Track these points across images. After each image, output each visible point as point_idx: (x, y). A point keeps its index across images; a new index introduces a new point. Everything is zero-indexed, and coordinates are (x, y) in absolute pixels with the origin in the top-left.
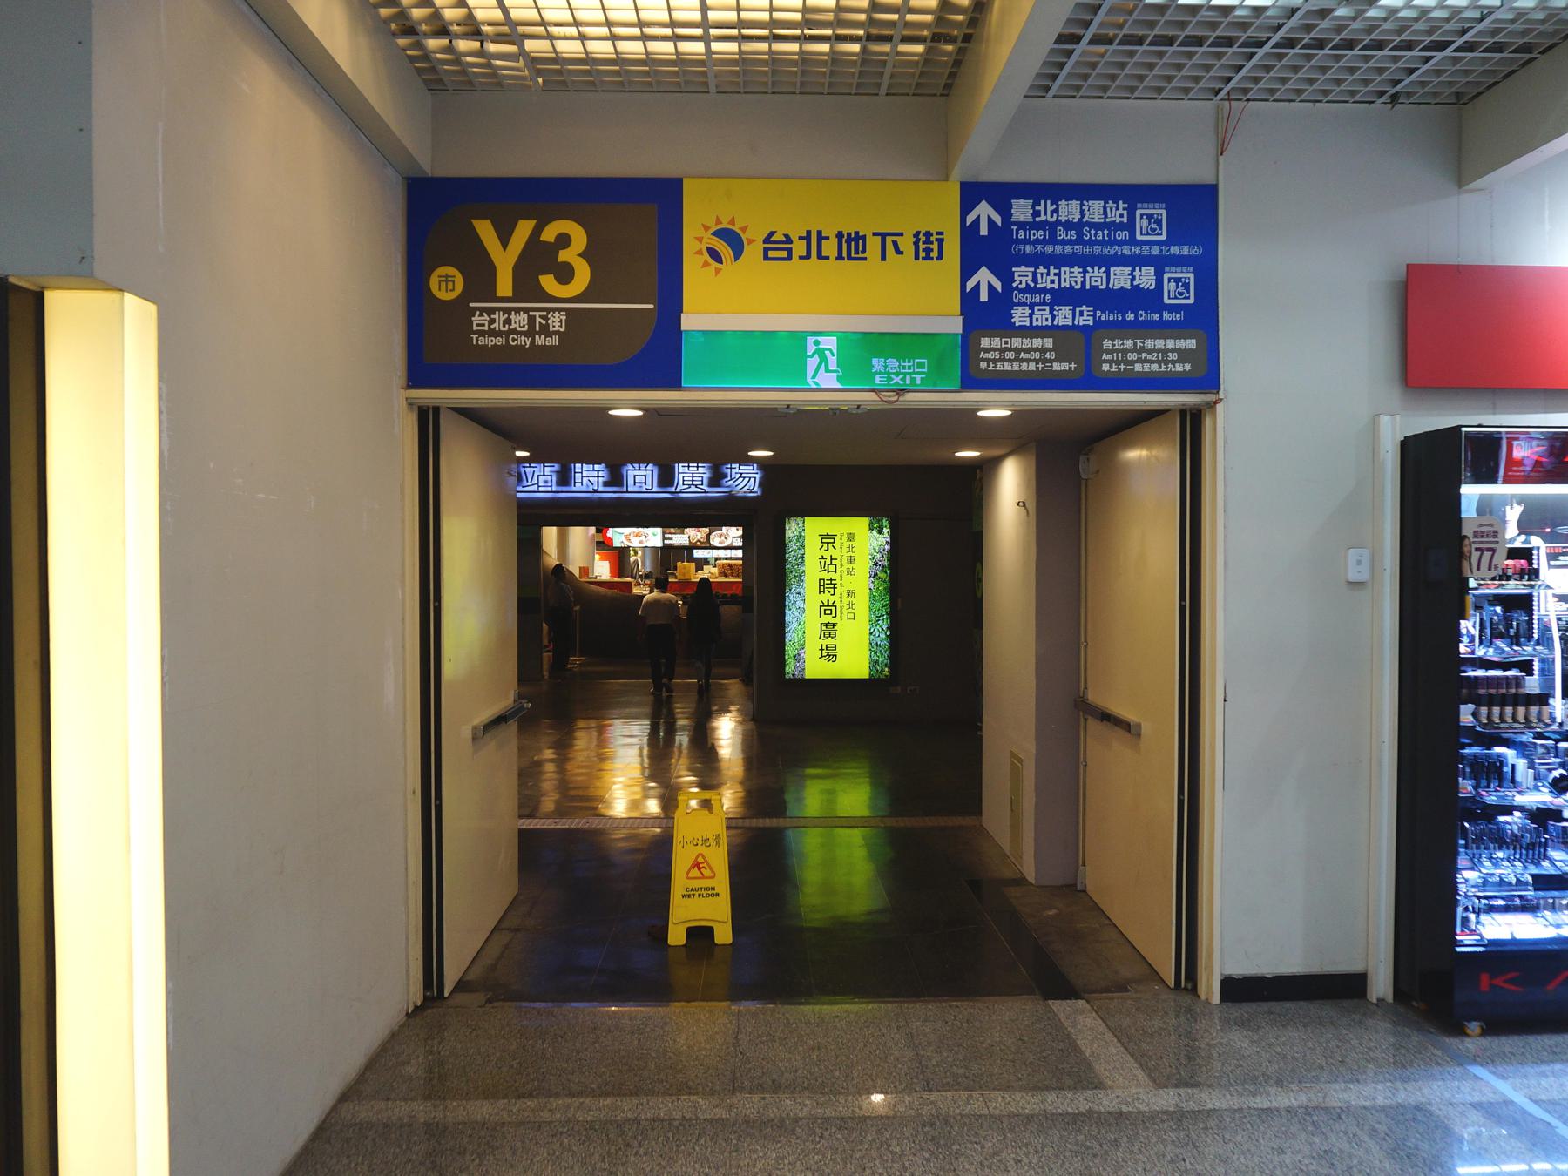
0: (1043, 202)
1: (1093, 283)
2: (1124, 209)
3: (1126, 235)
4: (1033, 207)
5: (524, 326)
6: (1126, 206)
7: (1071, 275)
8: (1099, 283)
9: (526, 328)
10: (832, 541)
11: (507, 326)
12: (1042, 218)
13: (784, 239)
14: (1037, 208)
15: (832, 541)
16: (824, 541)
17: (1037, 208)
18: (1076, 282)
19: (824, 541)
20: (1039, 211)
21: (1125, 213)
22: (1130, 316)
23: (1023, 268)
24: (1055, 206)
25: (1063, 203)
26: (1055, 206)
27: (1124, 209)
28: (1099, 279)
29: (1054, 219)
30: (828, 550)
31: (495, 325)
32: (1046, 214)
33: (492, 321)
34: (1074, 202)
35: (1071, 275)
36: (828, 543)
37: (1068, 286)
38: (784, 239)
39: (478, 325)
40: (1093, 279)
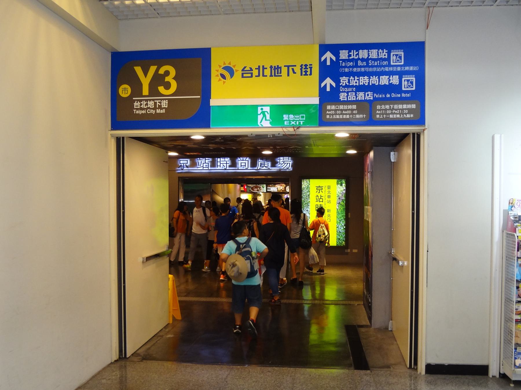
0: (352, 51)
1: (373, 83)
2: (386, 52)
3: (386, 63)
4: (348, 53)
5: (153, 106)
6: (387, 51)
7: (364, 80)
8: (375, 83)
9: (153, 107)
10: (321, 189)
11: (146, 106)
12: (382, 108)
13: (250, 69)
14: (350, 53)
15: (321, 189)
16: (318, 189)
17: (350, 53)
18: (366, 82)
19: (318, 189)
20: (351, 55)
21: (386, 54)
22: (388, 96)
23: (344, 77)
24: (357, 52)
25: (361, 51)
26: (357, 52)
27: (386, 52)
28: (375, 81)
29: (357, 58)
30: (319, 193)
31: (142, 106)
32: (353, 56)
33: (141, 105)
34: (365, 50)
35: (364, 80)
36: (319, 190)
37: (363, 84)
38: (250, 69)
39: (136, 106)
40: (373, 81)
